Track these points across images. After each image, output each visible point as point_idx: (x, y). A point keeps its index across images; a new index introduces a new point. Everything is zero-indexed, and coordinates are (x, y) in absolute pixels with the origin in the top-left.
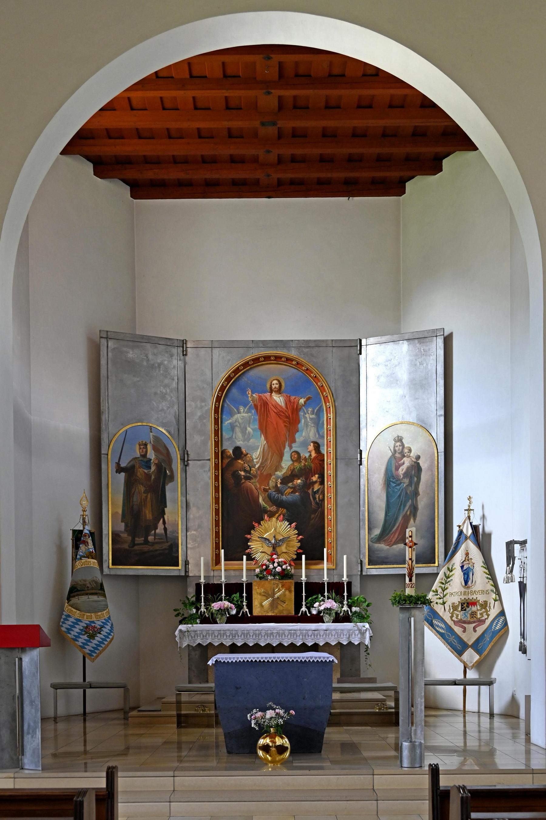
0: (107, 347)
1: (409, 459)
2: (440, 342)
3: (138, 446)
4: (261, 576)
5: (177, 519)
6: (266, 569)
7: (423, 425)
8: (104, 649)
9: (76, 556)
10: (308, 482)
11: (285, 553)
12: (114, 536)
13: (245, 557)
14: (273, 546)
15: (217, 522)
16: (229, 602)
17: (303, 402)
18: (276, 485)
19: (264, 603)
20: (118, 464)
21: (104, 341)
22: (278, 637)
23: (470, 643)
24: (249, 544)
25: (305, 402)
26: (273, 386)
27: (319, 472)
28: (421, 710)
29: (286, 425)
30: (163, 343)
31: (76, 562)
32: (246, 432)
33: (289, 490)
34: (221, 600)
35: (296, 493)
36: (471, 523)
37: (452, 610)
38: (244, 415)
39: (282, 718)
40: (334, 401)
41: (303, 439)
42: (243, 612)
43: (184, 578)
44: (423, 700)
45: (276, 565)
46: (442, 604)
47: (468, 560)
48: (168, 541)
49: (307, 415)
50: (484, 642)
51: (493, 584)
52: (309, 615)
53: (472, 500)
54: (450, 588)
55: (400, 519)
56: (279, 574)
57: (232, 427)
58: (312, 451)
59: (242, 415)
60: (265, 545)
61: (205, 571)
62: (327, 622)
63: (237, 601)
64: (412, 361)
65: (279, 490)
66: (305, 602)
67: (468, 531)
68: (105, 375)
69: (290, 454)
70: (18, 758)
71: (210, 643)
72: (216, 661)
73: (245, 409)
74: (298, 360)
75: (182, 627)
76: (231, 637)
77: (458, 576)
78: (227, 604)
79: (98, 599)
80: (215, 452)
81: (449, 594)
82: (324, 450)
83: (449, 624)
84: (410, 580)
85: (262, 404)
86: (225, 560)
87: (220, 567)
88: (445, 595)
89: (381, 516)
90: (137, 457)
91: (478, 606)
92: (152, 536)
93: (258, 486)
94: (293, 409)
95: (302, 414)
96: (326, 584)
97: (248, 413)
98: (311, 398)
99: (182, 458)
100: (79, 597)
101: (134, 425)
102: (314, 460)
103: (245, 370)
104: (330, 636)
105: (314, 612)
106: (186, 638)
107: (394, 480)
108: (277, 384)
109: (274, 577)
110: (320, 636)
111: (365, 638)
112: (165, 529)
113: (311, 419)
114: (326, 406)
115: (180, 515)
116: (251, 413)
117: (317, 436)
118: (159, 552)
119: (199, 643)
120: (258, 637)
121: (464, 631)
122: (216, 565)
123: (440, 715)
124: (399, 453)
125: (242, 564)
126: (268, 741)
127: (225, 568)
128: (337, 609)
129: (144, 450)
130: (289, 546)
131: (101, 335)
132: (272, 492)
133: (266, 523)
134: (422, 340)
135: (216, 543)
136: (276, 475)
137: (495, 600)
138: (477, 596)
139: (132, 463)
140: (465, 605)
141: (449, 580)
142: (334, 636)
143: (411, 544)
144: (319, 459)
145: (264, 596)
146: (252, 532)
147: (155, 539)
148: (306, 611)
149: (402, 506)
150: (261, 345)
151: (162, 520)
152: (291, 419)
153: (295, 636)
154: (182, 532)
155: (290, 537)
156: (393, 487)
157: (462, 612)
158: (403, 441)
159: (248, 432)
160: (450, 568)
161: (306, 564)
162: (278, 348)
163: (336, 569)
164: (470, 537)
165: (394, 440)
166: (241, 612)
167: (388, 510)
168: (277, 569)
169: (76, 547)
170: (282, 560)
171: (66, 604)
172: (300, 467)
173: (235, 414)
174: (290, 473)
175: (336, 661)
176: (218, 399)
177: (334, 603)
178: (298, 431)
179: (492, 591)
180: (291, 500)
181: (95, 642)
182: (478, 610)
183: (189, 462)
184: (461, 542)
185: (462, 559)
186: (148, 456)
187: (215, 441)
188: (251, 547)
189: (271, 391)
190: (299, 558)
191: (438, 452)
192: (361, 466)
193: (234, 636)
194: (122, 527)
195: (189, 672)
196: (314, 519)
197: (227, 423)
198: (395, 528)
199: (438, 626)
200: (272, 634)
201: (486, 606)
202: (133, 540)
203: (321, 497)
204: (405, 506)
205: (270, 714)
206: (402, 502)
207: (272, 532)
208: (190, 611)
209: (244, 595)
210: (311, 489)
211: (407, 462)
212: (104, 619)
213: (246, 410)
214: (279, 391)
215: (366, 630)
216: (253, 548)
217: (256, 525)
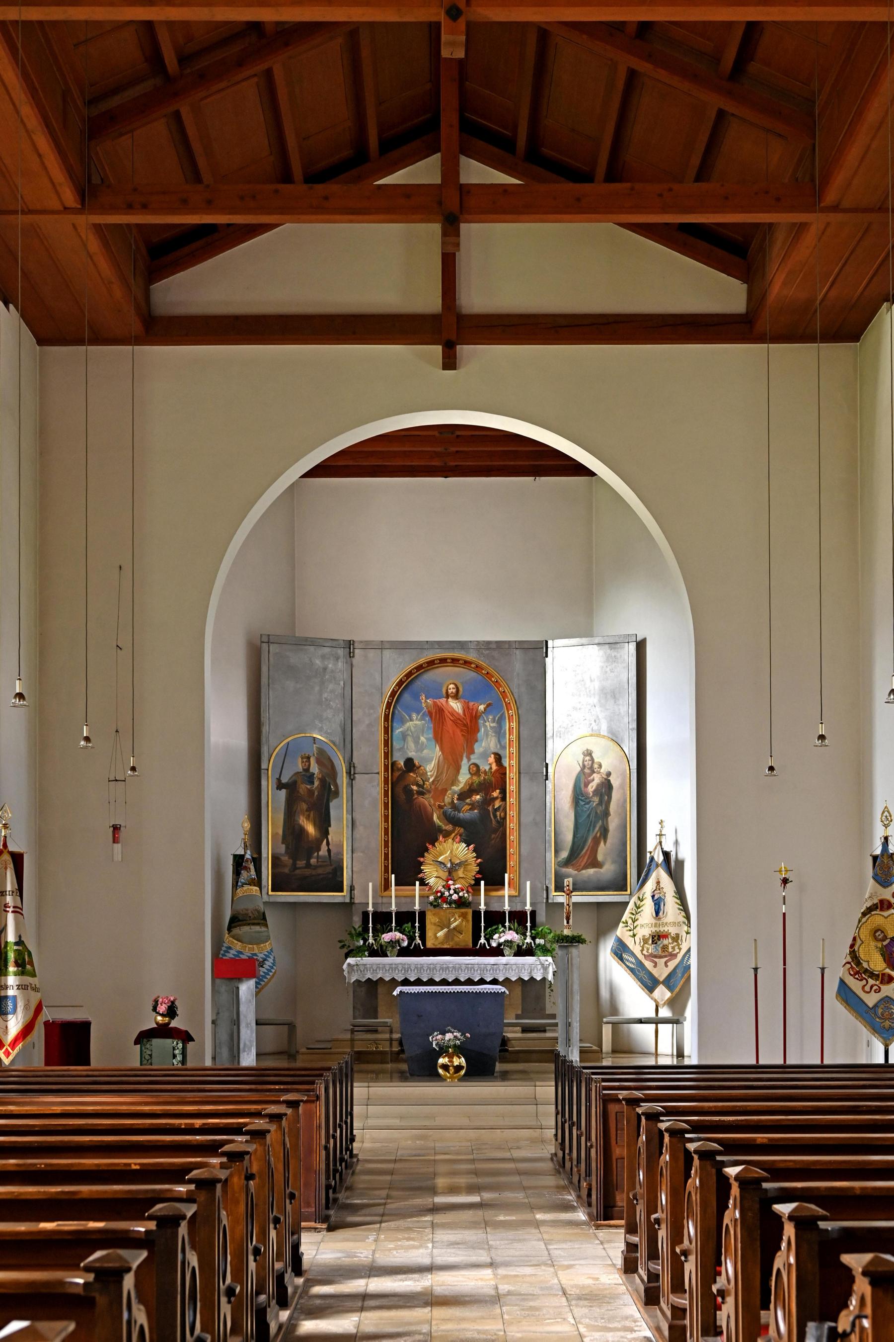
0: (269, 652)
1: (599, 776)
2: (632, 647)
5: (342, 840)
7: (614, 738)
8: (267, 983)
9: (237, 883)
10: (488, 797)
13: (417, 883)
15: (386, 842)
16: (401, 933)
17: (483, 709)
18: (453, 801)
19: (439, 935)
20: (279, 780)
21: (265, 646)
22: (454, 971)
23: (661, 979)
25: (485, 709)
26: (449, 690)
27: (500, 787)
28: (576, 1032)
31: (237, 889)
32: (418, 742)
37: (642, 943)
38: (417, 722)
39: (459, 1040)
40: (517, 709)
42: (415, 943)
43: (349, 906)
44: (578, 1024)
45: (452, 892)
46: (632, 937)
47: (659, 889)
49: (487, 724)
51: (685, 915)
52: (488, 948)
53: (664, 824)
55: (590, 840)
56: (455, 902)
57: (404, 736)
58: (492, 763)
59: (415, 722)
61: (373, 897)
62: (507, 956)
63: (409, 932)
64: (603, 667)
67: (659, 858)
68: (266, 683)
72: (401, 991)
75: (351, 960)
76: (403, 972)
77: (648, 906)
78: (398, 935)
80: (385, 764)
81: (639, 926)
82: (506, 763)
83: (640, 958)
84: (568, 922)
86: (396, 885)
89: (568, 837)
91: (670, 939)
92: (315, 858)
93: (432, 802)
94: (471, 714)
96: (507, 913)
99: (348, 771)
101: (296, 736)
103: (418, 673)
105: (494, 944)
107: (583, 798)
110: (500, 970)
111: (548, 973)
112: (329, 851)
114: (508, 714)
115: (345, 835)
117: (499, 746)
118: (322, 876)
119: (369, 978)
121: (655, 966)
124: (588, 768)
128: (518, 941)
129: (307, 764)
130: (466, 871)
131: (262, 640)
134: (613, 646)
135: (385, 865)
139: (294, 778)
140: (656, 938)
141: (639, 910)
142: (515, 970)
143: (568, 892)
147: (318, 861)
148: (485, 943)
149: (592, 828)
150: (437, 646)
151: (325, 841)
153: (472, 971)
154: (347, 853)
156: (582, 806)
158: (593, 755)
160: (641, 898)
161: (485, 890)
162: (456, 650)
163: (519, 896)
165: (583, 753)
166: (413, 944)
167: (577, 831)
168: (453, 897)
169: (237, 873)
171: (227, 935)
174: (468, 787)
175: (507, 992)
176: (389, 705)
177: (516, 935)
178: (477, 741)
179: (684, 923)
182: (669, 943)
183: (356, 775)
184: (652, 870)
186: (311, 770)
187: (384, 752)
188: (425, 871)
189: (447, 696)
190: (478, 884)
191: (630, 769)
192: (547, 781)
193: (406, 970)
194: (282, 849)
195: (354, 1011)
197: (397, 731)
198: (584, 851)
199: (628, 960)
200: (448, 968)
202: (294, 864)
203: (502, 814)
204: (594, 827)
205: (449, 1036)
206: (591, 822)
207: (447, 855)
208: (356, 943)
209: (417, 924)
210: (491, 807)
211: (597, 779)
213: (419, 717)
214: (456, 696)
215: (549, 965)
217: (430, 846)
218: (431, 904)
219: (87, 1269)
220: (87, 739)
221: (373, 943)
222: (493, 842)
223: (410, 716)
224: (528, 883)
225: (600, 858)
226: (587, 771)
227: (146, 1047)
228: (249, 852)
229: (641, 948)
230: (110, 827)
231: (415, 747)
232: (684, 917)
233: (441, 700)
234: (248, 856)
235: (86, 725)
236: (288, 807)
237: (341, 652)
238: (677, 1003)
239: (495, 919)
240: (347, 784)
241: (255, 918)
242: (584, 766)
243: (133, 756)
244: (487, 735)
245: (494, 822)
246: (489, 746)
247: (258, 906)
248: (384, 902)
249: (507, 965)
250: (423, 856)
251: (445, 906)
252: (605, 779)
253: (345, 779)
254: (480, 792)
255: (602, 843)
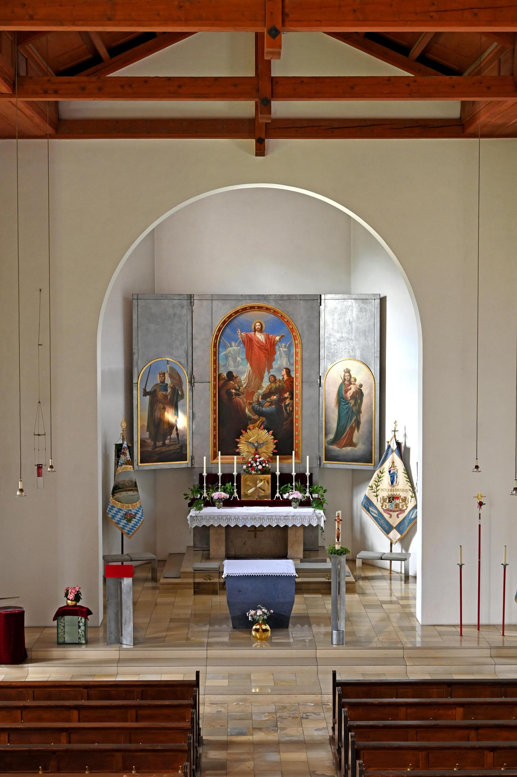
1: (354, 386)
3: (158, 375)
6: (251, 466)
9: (118, 462)
10: (281, 398)
11: (264, 452)
12: (142, 442)
17: (278, 339)
18: (258, 400)
22: (259, 521)
23: (394, 526)
24: (238, 445)
25: (280, 339)
26: (256, 327)
30: (177, 298)
32: (236, 361)
36: (396, 440)
37: (382, 501)
40: (301, 340)
42: (234, 497)
45: (258, 464)
47: (394, 467)
48: (180, 442)
49: (281, 349)
50: (404, 525)
51: (410, 485)
52: (281, 499)
53: (397, 423)
54: (381, 485)
55: (348, 429)
56: (260, 470)
57: (227, 357)
59: (233, 348)
67: (394, 446)
70: (119, 638)
71: (212, 525)
77: (386, 478)
79: (133, 494)
82: (293, 374)
84: (338, 540)
87: (217, 461)
88: (378, 490)
89: (334, 425)
90: (158, 383)
91: (400, 500)
92: (168, 440)
95: (278, 348)
99: (190, 381)
100: (121, 493)
101: (156, 360)
103: (236, 315)
104: (296, 520)
106: (195, 521)
110: (289, 520)
111: (320, 522)
112: (178, 434)
113: (284, 351)
117: (288, 364)
118: (173, 451)
119: (204, 525)
120: (246, 521)
121: (391, 517)
123: (373, 576)
126: (258, 627)
128: (301, 498)
129: (163, 378)
131: (134, 298)
132: (255, 405)
134: (365, 301)
137: (412, 497)
138: (399, 493)
141: (380, 479)
142: (299, 520)
143: (339, 520)
146: (241, 437)
147: (170, 442)
148: (279, 496)
150: (248, 298)
152: (269, 351)
157: (389, 503)
158: (350, 372)
160: (382, 471)
162: (260, 301)
164: (395, 450)
165: (344, 371)
167: (340, 422)
168: (259, 467)
169: (118, 456)
171: (111, 498)
173: (229, 347)
174: (268, 391)
176: (217, 337)
178: (274, 360)
181: (131, 524)
184: (389, 454)
185: (389, 466)
186: (166, 382)
187: (214, 368)
188: (240, 448)
189: (255, 331)
191: (375, 383)
194: (147, 435)
197: (222, 354)
199: (373, 512)
201: (406, 500)
204: (351, 420)
205: (259, 612)
206: (349, 417)
207: (255, 438)
209: (235, 484)
210: (284, 403)
211: (353, 389)
212: (138, 508)
214: (261, 331)
215: (322, 516)
218: (244, 470)
220: (21, 490)
221: (206, 497)
222: (284, 427)
224: (308, 457)
225: (355, 440)
226: (346, 382)
227: (61, 621)
228: (125, 443)
229: (381, 505)
230: (35, 465)
231: (234, 364)
232: (410, 487)
233: (251, 333)
234: (125, 445)
235: (21, 481)
236: (151, 406)
237: (185, 302)
238: (405, 541)
239: (286, 478)
240: (189, 389)
241: (130, 487)
242: (345, 379)
243: (51, 459)
244: (281, 357)
245: (285, 413)
247: (132, 478)
248: (213, 467)
249: (294, 516)
250: (239, 438)
251: (253, 472)
252: (358, 389)
253: (188, 387)
255: (356, 431)
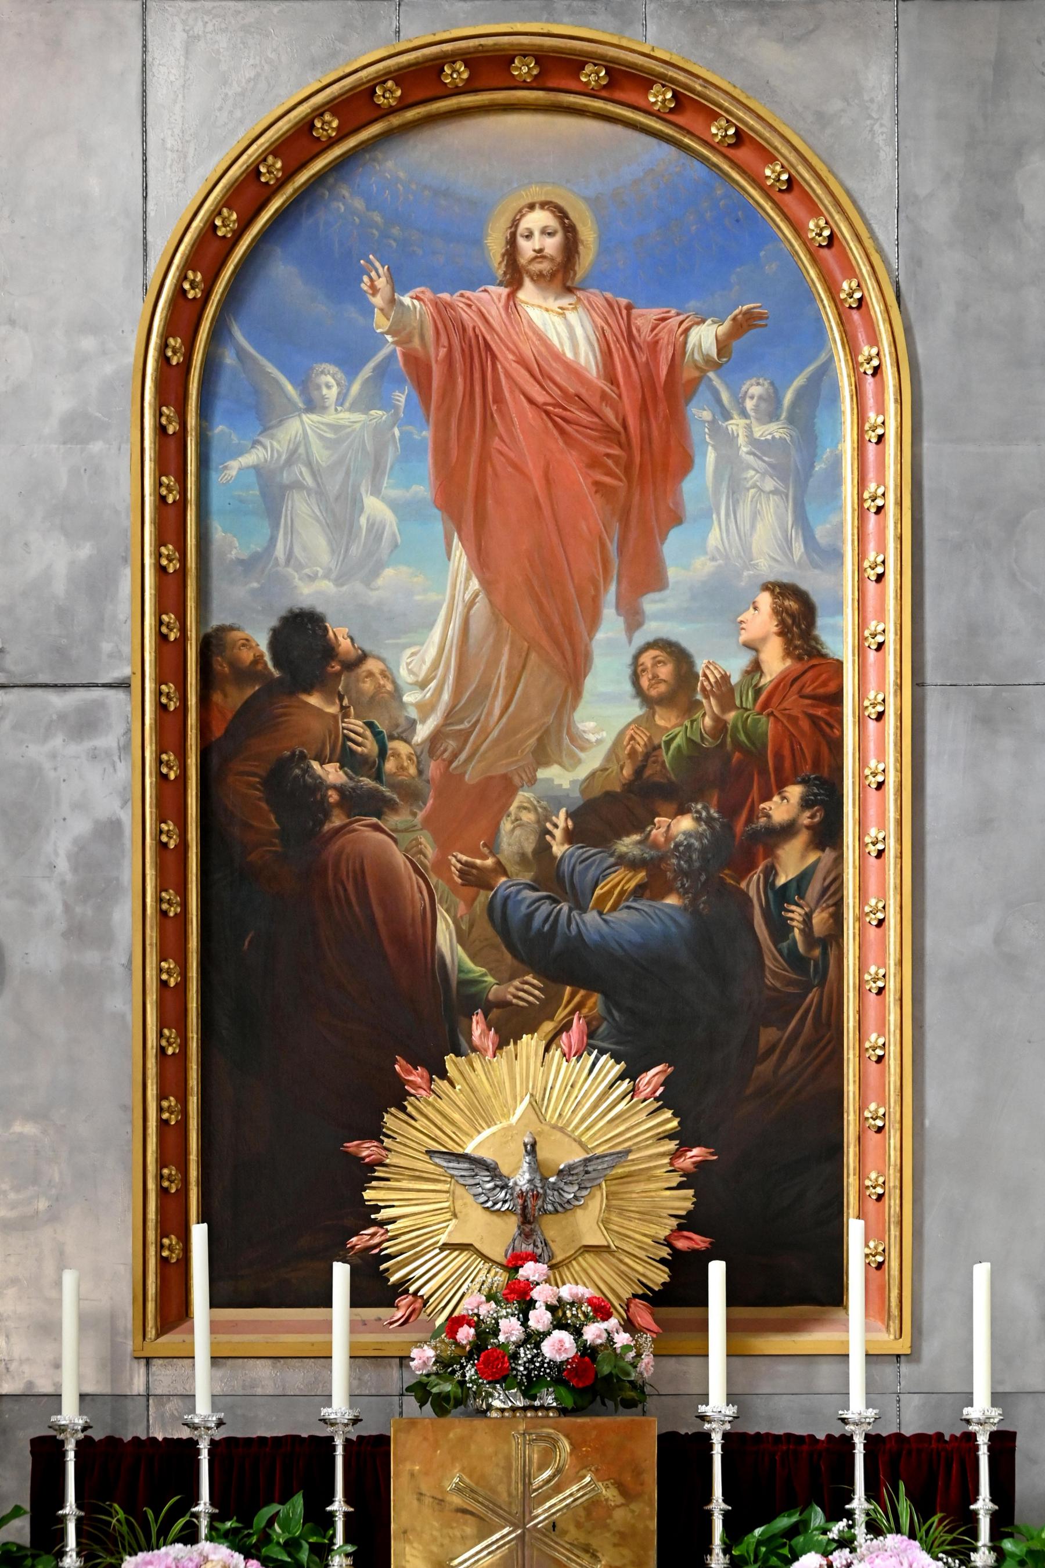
4: (447, 1387)
10: (739, 827)
13: (341, 1273)
14: (524, 1208)
18: (543, 849)
24: (367, 1195)
25: (723, 346)
26: (522, 242)
27: (807, 769)
29: (607, 480)
33: (628, 880)
34: (190, 1537)
35: (663, 896)
38: (345, 417)
40: (908, 330)
41: (711, 566)
45: (540, 1318)
49: (736, 425)
58: (764, 640)
60: (470, 1199)
63: (292, 1545)
65: (559, 878)
66: (726, 1551)
69: (628, 659)
73: (351, 382)
74: (681, 77)
85: (457, 355)
86: (214, 1303)
94: (649, 380)
95: (707, 415)
97: (366, 410)
98: (761, 316)
102: (775, 700)
103: (352, 142)
108: (551, 234)
109: (527, 1394)
113: (759, 447)
116: (387, 404)
117: (798, 549)
122: (162, 1331)
125: (327, 1326)
127: (213, 1345)
130: (622, 1211)
133: (477, 1065)
135: (163, 1192)
136: (537, 786)
144: (808, 690)
145: (464, 1511)
146: (391, 1121)
152: (635, 440)
155: (628, 1152)
159: (371, 525)
161: (732, 1326)
163: (913, 1356)
168: (548, 1349)
170: (585, 1291)
172: (689, 740)
173: (291, 410)
174: (627, 772)
178: (677, 519)
180: (636, 938)
188: (384, 1214)
196: (775, 1057)
197: (234, 466)
203: (820, 919)
207: (513, 1120)
209: (339, 1506)
210: (757, 876)
213: (355, 388)
216: (392, 1221)
217: (417, 1076)
218: (421, 1390)
219: (814, 978)
223: (305, 384)
244: (736, 490)
246: (746, 548)
254: (698, 794)
